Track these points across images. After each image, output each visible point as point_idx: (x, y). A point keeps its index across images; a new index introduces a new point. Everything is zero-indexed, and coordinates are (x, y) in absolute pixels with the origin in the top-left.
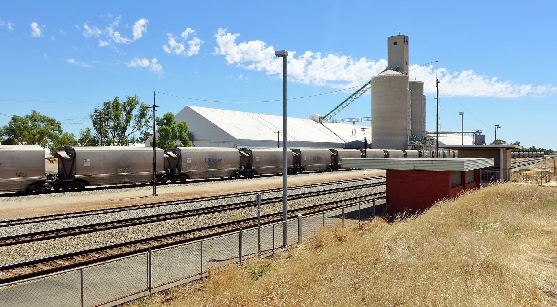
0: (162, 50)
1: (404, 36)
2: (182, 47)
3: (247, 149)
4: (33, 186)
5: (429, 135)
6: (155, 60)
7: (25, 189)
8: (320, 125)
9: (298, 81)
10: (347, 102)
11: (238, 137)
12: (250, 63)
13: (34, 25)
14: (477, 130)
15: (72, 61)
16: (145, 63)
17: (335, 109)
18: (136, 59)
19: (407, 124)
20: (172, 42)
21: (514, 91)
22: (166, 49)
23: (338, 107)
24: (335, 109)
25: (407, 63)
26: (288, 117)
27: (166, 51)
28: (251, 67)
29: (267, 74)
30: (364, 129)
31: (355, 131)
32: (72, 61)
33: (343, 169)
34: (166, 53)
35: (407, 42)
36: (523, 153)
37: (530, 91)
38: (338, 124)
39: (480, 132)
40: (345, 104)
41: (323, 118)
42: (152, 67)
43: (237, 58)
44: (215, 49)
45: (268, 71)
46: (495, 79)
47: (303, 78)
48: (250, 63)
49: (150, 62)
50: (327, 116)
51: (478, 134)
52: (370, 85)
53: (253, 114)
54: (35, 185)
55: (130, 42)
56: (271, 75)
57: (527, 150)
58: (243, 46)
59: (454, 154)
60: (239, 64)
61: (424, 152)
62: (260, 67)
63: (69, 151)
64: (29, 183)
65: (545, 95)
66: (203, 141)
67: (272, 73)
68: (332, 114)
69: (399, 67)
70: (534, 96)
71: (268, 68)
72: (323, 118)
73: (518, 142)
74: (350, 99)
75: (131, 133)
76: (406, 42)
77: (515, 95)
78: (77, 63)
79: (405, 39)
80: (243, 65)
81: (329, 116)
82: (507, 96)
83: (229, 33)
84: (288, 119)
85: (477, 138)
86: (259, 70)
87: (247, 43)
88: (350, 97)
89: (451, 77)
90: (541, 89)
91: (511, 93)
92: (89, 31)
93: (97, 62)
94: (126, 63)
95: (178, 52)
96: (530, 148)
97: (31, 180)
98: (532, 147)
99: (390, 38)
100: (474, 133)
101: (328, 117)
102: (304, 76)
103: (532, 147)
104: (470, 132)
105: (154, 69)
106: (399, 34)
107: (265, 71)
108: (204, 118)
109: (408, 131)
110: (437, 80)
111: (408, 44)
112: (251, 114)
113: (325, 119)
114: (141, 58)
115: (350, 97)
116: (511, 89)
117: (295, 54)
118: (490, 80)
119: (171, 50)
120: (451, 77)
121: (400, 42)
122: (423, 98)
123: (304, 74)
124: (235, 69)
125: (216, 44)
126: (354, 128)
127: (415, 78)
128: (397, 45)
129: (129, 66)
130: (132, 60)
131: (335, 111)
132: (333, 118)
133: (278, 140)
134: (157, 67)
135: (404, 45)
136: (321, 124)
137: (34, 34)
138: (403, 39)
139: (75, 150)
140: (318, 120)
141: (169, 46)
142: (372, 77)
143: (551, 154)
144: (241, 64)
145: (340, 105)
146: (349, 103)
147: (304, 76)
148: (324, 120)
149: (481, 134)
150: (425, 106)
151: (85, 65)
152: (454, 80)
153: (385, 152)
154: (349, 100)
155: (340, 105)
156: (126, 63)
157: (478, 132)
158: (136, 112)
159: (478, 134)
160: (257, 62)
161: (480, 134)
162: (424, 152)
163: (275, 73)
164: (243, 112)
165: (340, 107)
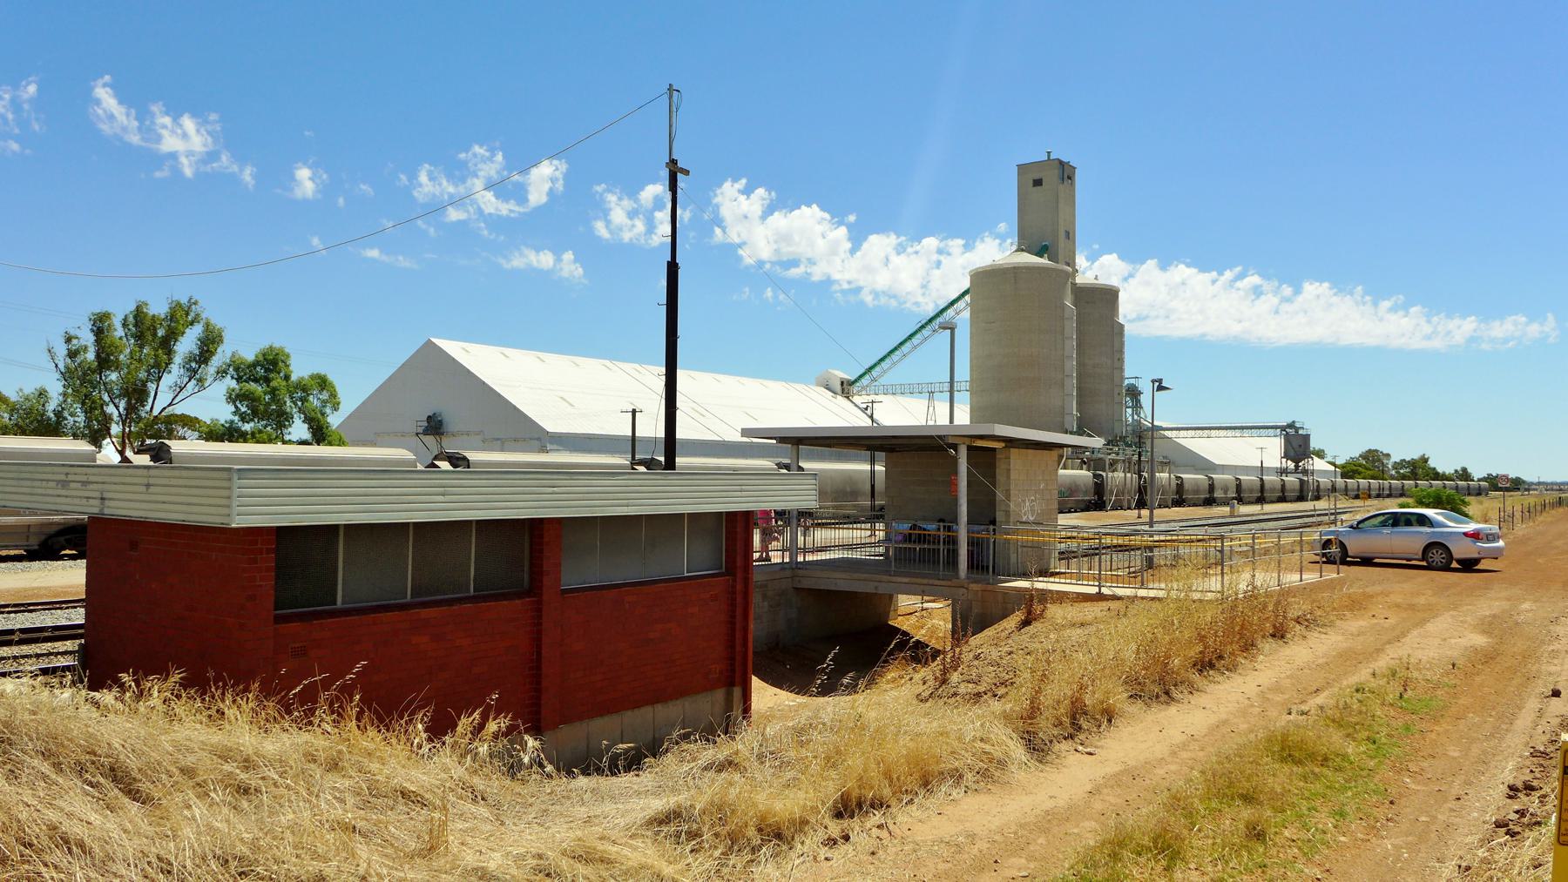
0: (591, 231)
1: (1061, 163)
2: (640, 226)
3: (458, 453)
4: (62, 539)
5: (1162, 432)
6: (568, 256)
7: (39, 545)
8: (841, 400)
9: (908, 305)
10: (915, 340)
11: (551, 427)
12: (794, 263)
13: (303, 174)
14: (1290, 421)
15: (374, 253)
16: (546, 260)
17: (882, 360)
18: (526, 251)
19: (1064, 400)
20: (618, 215)
21: (1433, 333)
22: (600, 228)
23: (891, 352)
24: (882, 360)
25: (1071, 235)
26: (681, 369)
27: (599, 234)
28: (795, 272)
29: (835, 287)
30: (870, 405)
31: (933, 418)
32: (374, 253)
33: (1240, 516)
34: (600, 238)
35: (1069, 178)
36: (1466, 485)
37: (1475, 334)
38: (900, 398)
39: (1297, 425)
40: (908, 345)
41: (852, 383)
42: (561, 269)
43: (765, 253)
44: (713, 232)
45: (837, 282)
46: (1386, 304)
47: (920, 299)
48: (794, 263)
49: (558, 260)
50: (861, 376)
51: (1291, 431)
52: (967, 298)
53: (806, 388)
54: (67, 537)
55: (519, 212)
56: (843, 292)
57: (1444, 477)
58: (778, 220)
59: (1213, 483)
60: (768, 266)
61: (1107, 476)
62: (817, 273)
63: (455, 461)
64: (54, 529)
65: (1511, 344)
66: (466, 436)
67: (846, 286)
68: (875, 373)
69: (1045, 245)
70: (1484, 346)
71: (837, 276)
72: (852, 383)
73: (1426, 457)
74: (924, 331)
75: (170, 405)
76: (1066, 176)
77: (1437, 344)
78: (385, 258)
79: (1065, 172)
80: (778, 268)
81: (867, 377)
82: (1417, 343)
83: (934, 236)
84: (682, 375)
85: (1290, 443)
86: (816, 278)
87: (920, 242)
88: (923, 327)
89: (1275, 300)
90: (1504, 328)
91: (1428, 337)
92: (427, 184)
93: (435, 256)
94: (502, 261)
95: (627, 236)
96: (1456, 471)
97: (58, 524)
98: (1459, 469)
99: (1022, 168)
100: (1283, 428)
101: (865, 381)
102: (924, 294)
103: (1459, 469)
104: (1272, 427)
105: (565, 274)
106: (1049, 156)
107: (828, 282)
108: (469, 371)
109: (1067, 419)
110: (673, 162)
111: (1072, 184)
112: (627, 366)
113: (858, 384)
114: (538, 250)
115: (923, 327)
116: (1428, 329)
117: (567, 169)
118: (1375, 304)
119: (611, 232)
120: (1275, 300)
121: (1051, 177)
122: (1116, 331)
123: (920, 291)
124: (762, 275)
125: (718, 221)
126: (931, 409)
127: (1097, 276)
128: (1041, 185)
129: (507, 266)
130: (517, 254)
131: (884, 365)
132: (882, 381)
133: (661, 434)
134: (569, 266)
135: (1061, 187)
136: (848, 398)
137: (298, 194)
138: (1056, 171)
139: (468, 460)
140: (838, 388)
141: (608, 223)
142: (970, 272)
143: (1519, 489)
144: (773, 263)
145: (896, 349)
146: (919, 341)
147: (924, 294)
148: (855, 389)
149: (1301, 432)
150: (1121, 351)
151: (403, 262)
152: (1285, 307)
153: (1095, 476)
154: (918, 336)
155: (896, 349)
156: (502, 261)
157: (1291, 425)
158: (187, 344)
159: (1291, 431)
160: (811, 262)
161: (1297, 432)
162: (1107, 476)
163: (853, 286)
164: (784, 383)
165: (897, 353)
